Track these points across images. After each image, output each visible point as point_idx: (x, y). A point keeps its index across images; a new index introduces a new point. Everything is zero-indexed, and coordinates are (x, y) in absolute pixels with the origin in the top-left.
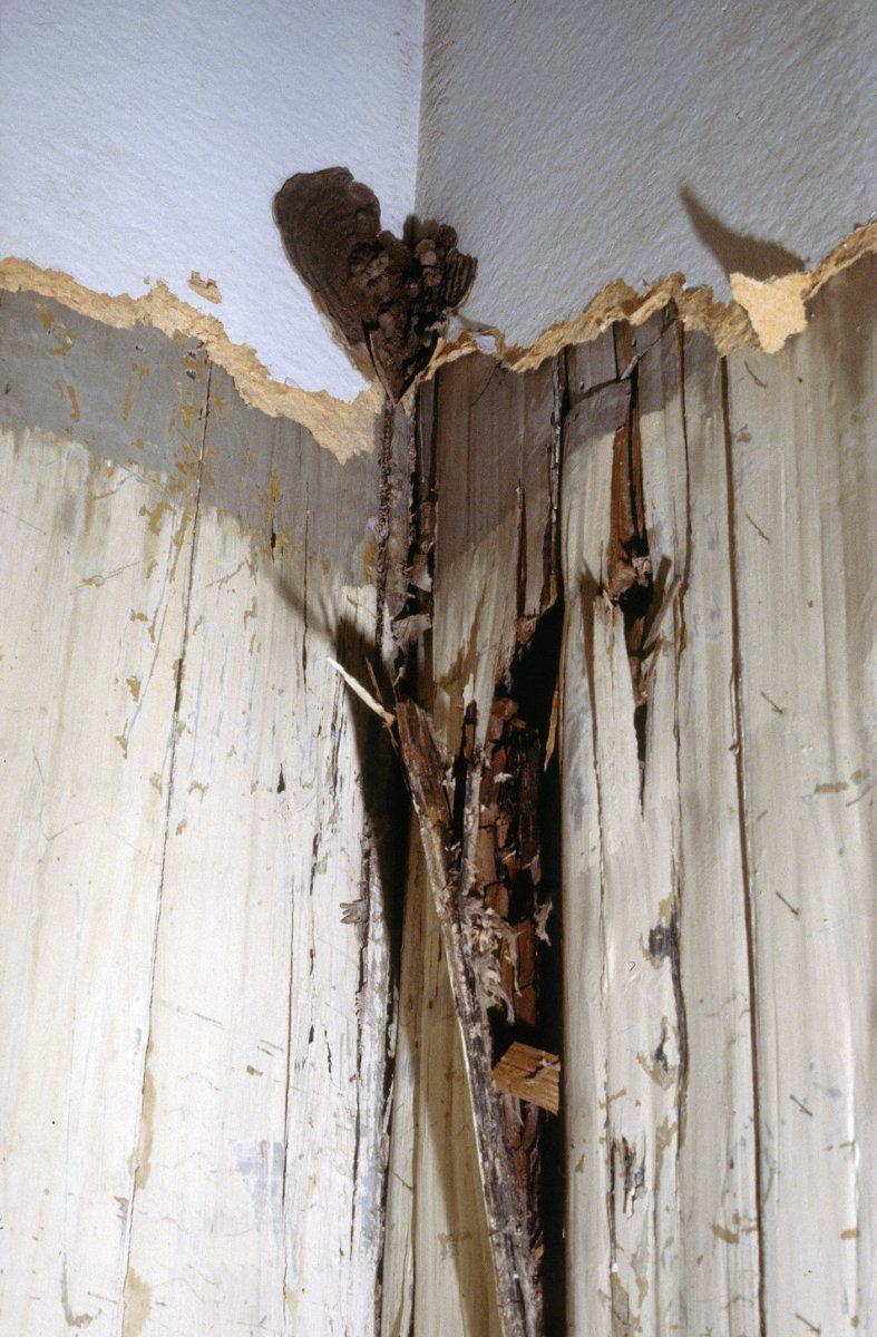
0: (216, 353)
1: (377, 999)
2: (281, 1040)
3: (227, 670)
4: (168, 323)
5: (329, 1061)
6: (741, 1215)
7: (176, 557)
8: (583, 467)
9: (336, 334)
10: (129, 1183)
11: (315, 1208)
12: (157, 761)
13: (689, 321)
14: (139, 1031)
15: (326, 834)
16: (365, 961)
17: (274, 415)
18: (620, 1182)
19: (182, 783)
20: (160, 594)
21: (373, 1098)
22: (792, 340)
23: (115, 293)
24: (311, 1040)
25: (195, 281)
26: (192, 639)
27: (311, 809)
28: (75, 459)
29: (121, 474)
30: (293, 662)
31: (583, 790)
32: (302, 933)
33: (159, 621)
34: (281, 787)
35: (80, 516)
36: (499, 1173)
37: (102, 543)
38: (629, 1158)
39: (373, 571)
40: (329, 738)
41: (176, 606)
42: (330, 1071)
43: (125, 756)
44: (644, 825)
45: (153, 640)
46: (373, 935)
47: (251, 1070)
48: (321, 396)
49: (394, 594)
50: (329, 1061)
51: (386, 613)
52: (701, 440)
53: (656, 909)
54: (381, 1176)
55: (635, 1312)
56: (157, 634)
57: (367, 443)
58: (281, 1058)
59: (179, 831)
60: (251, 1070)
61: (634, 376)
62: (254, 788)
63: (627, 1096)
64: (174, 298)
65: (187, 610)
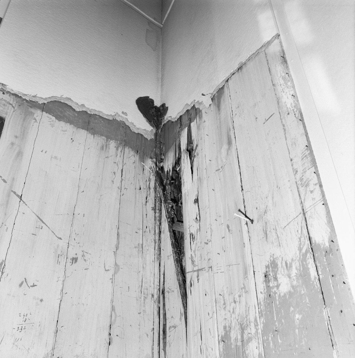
0: (127, 124)
1: (158, 222)
4: (118, 119)
8: (183, 133)
9: (147, 121)
10: (116, 249)
12: (119, 184)
13: (197, 107)
14: (117, 225)
15: (148, 197)
17: (137, 133)
18: (192, 239)
19: (123, 189)
20: (119, 159)
21: (158, 237)
22: (210, 105)
23: (109, 114)
24: (147, 228)
25: (123, 113)
27: (145, 192)
28: (103, 139)
29: (111, 141)
31: (184, 181)
32: (144, 211)
34: (140, 189)
36: (173, 242)
37: (108, 152)
38: (193, 236)
41: (121, 161)
44: (193, 184)
47: (136, 232)
48: (145, 130)
49: (158, 160)
52: (199, 124)
55: (194, 259)
56: (118, 165)
57: (153, 137)
58: (141, 231)
59: (123, 195)
60: (136, 232)
61: (190, 118)
62: (135, 189)
64: (119, 115)
65: (123, 162)
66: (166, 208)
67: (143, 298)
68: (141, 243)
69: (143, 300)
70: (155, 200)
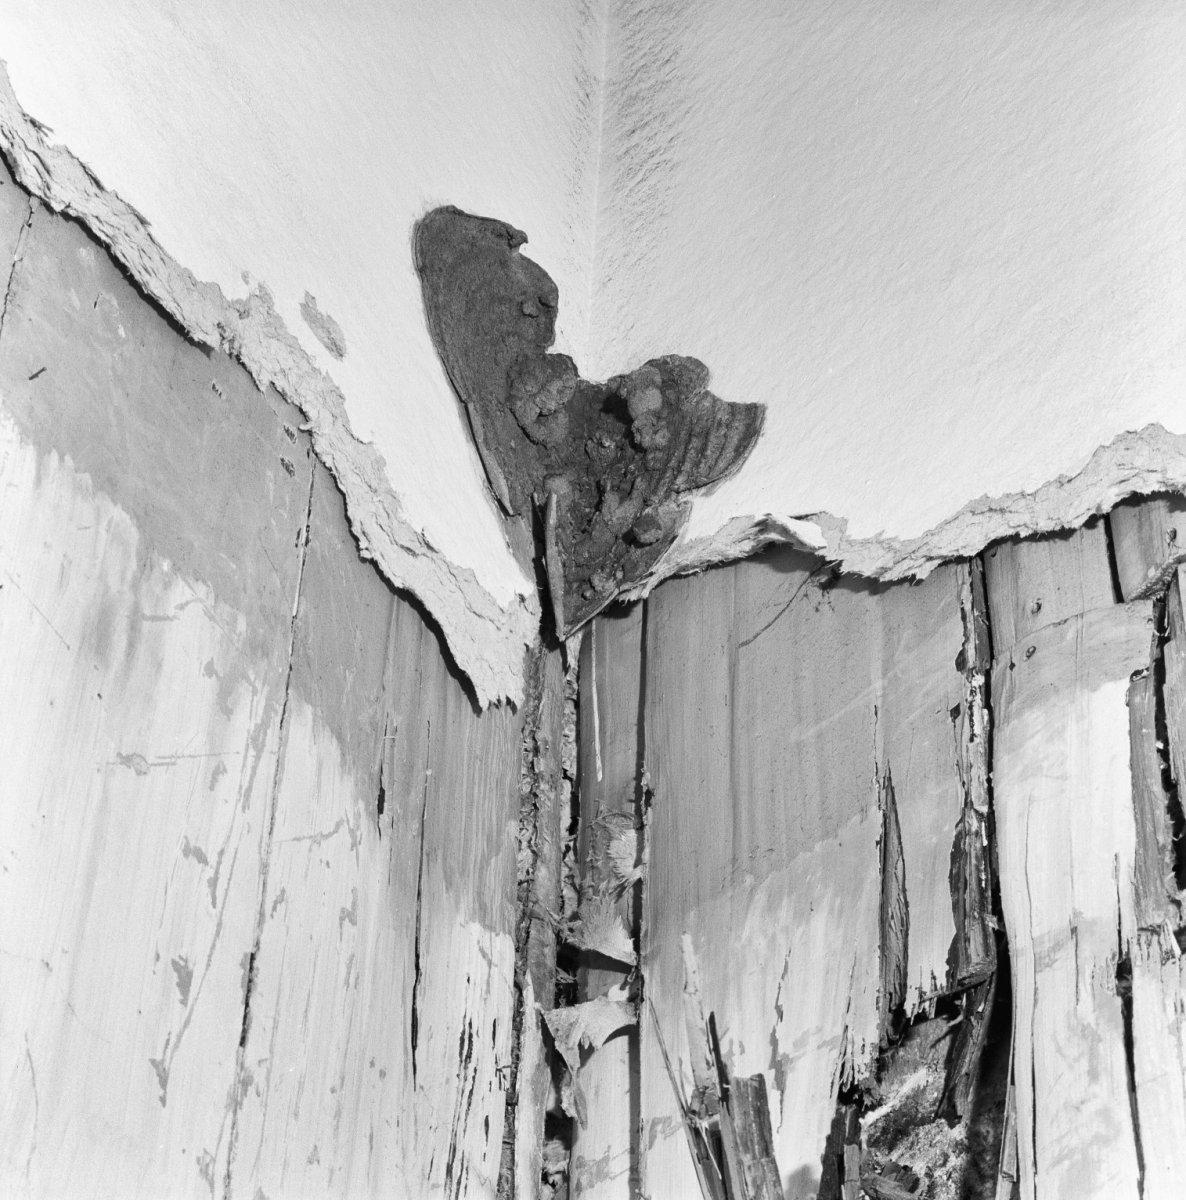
3: (314, 1000)
7: (254, 769)
26: (269, 923)
30: (401, 1028)
33: (224, 870)
35: (120, 640)
39: (513, 918)
43: (163, 1100)
45: (214, 904)
51: (529, 994)
56: (220, 893)
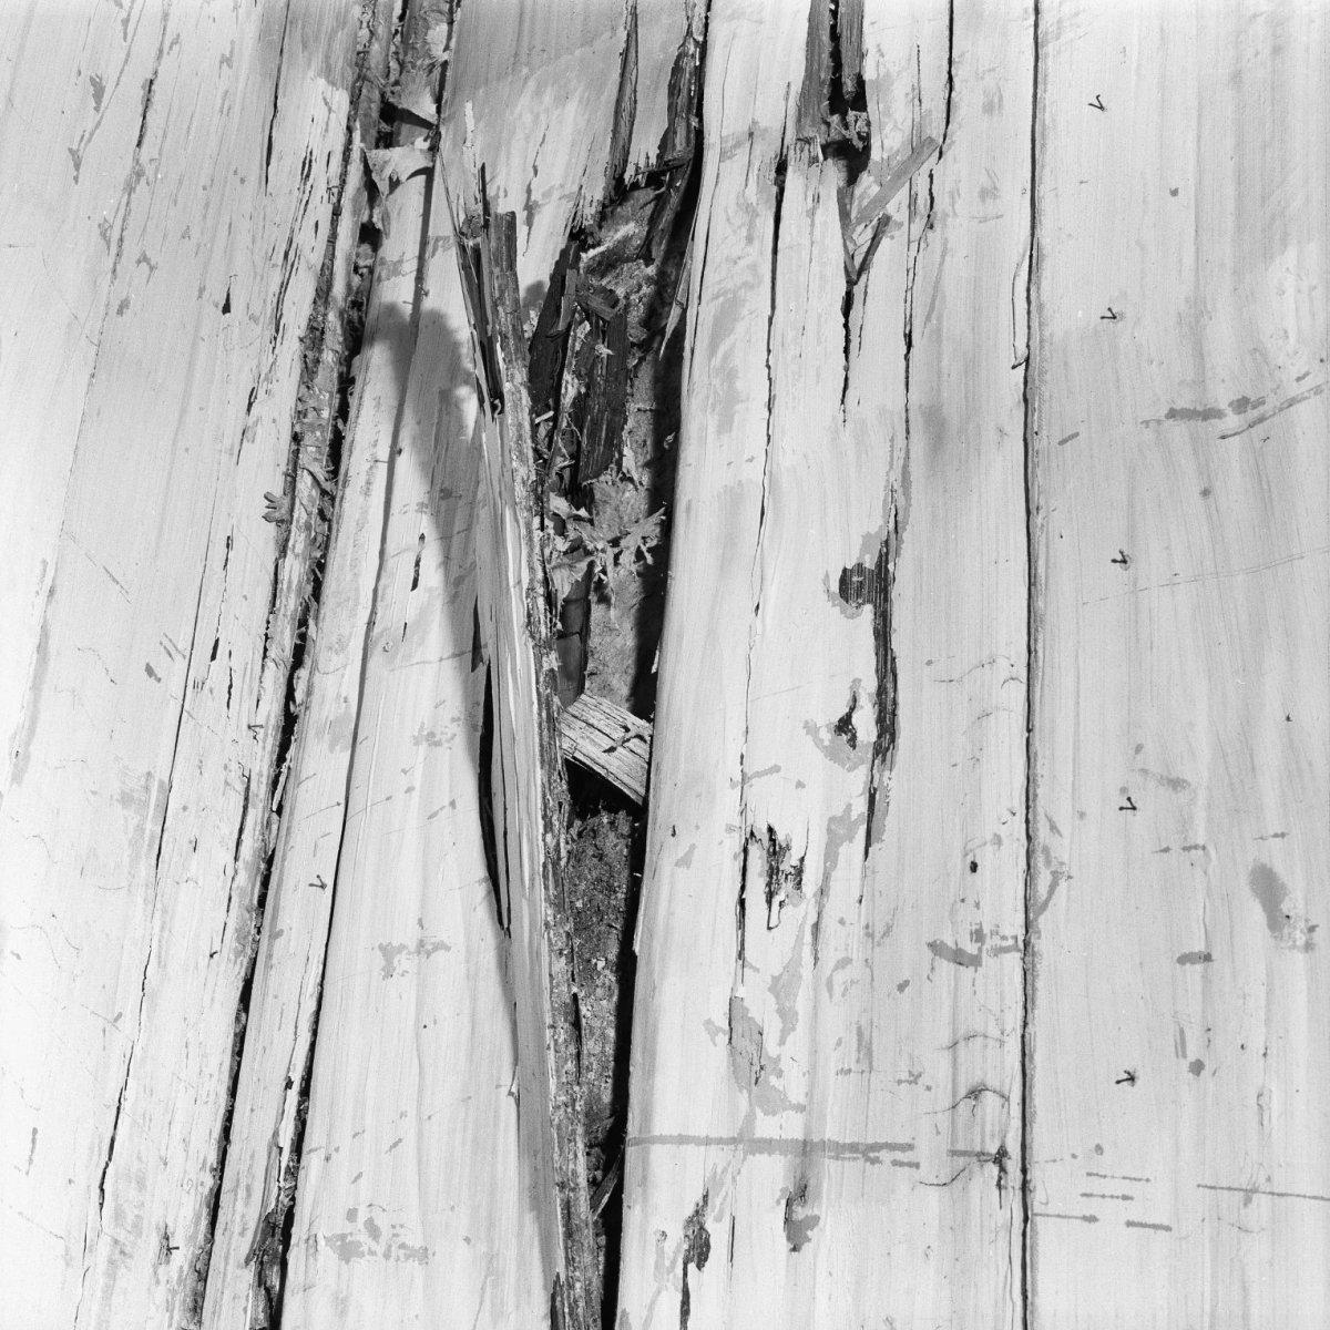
2: (184, 645)
5: (229, 693)
6: (986, 931)
11: (191, 884)
16: (280, 577)
34: (226, 309)
40: (279, 268)
42: (228, 706)
43: (76, 179)
46: (294, 546)
47: (150, 671)
50: (229, 693)
51: (357, 136)
53: (857, 542)
54: (263, 866)
63: (782, 773)
66: (536, 557)
67: (103, 1249)
68: (162, 774)
69: (102, 1266)
70: (296, 438)
